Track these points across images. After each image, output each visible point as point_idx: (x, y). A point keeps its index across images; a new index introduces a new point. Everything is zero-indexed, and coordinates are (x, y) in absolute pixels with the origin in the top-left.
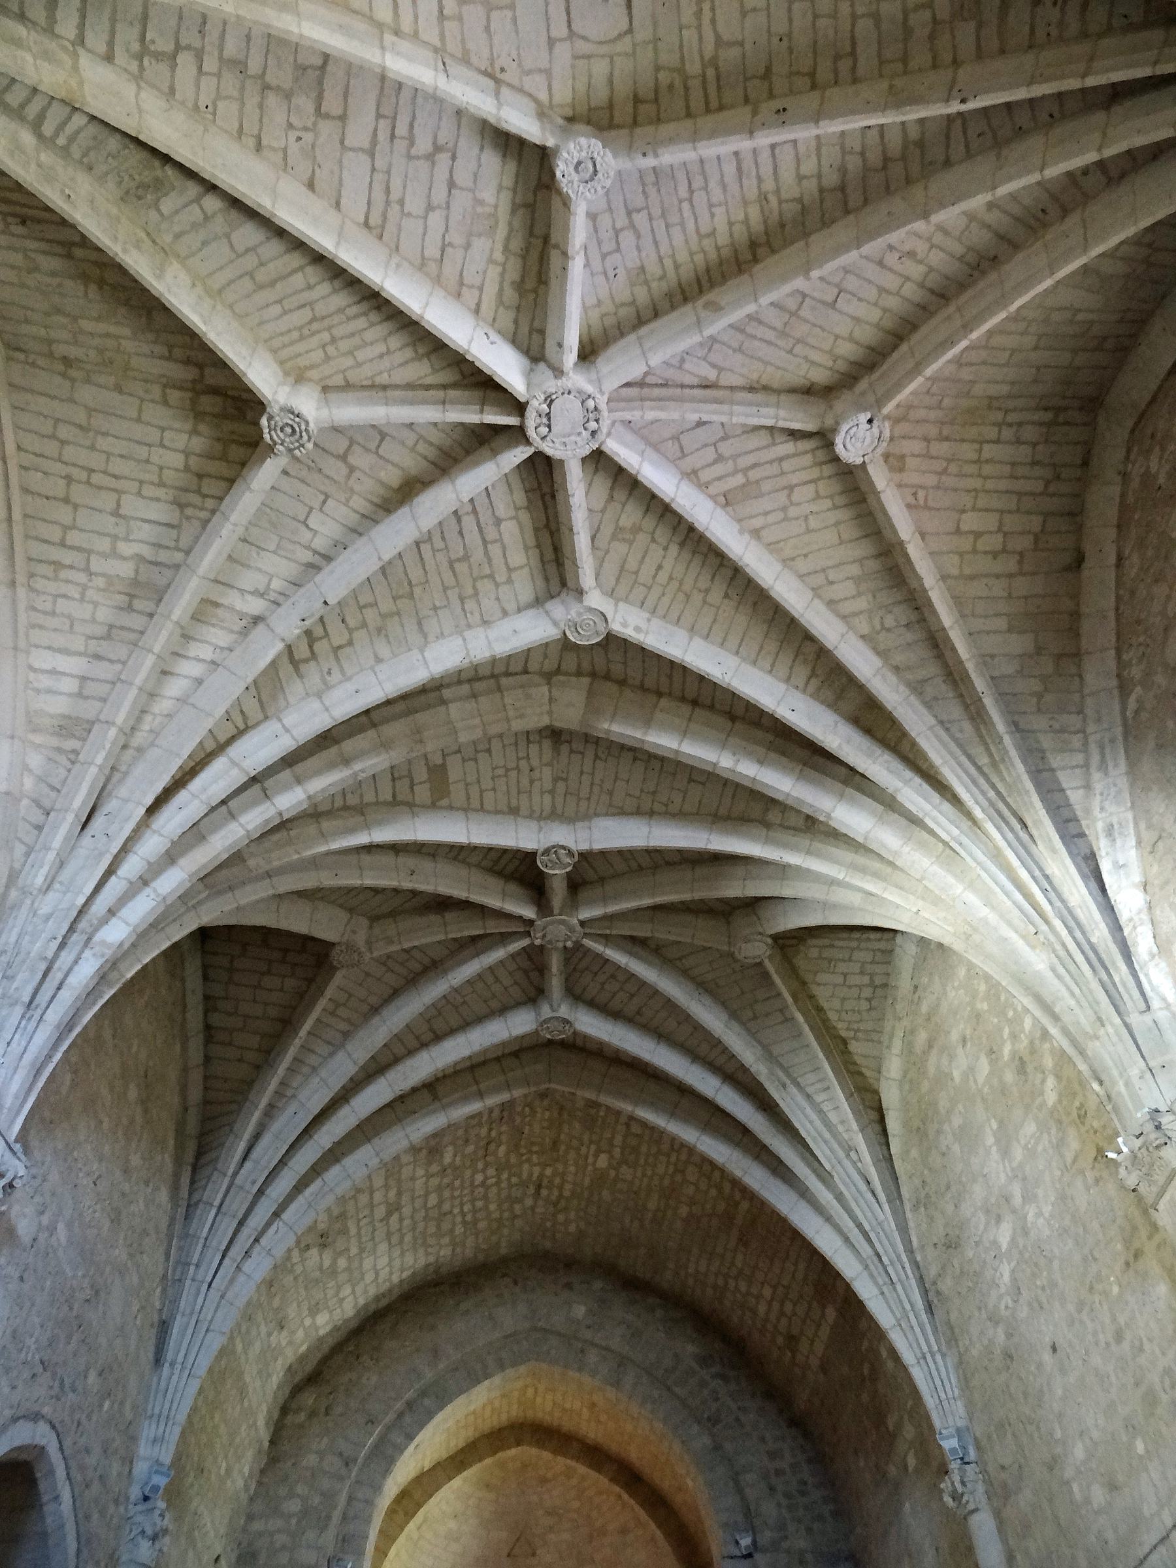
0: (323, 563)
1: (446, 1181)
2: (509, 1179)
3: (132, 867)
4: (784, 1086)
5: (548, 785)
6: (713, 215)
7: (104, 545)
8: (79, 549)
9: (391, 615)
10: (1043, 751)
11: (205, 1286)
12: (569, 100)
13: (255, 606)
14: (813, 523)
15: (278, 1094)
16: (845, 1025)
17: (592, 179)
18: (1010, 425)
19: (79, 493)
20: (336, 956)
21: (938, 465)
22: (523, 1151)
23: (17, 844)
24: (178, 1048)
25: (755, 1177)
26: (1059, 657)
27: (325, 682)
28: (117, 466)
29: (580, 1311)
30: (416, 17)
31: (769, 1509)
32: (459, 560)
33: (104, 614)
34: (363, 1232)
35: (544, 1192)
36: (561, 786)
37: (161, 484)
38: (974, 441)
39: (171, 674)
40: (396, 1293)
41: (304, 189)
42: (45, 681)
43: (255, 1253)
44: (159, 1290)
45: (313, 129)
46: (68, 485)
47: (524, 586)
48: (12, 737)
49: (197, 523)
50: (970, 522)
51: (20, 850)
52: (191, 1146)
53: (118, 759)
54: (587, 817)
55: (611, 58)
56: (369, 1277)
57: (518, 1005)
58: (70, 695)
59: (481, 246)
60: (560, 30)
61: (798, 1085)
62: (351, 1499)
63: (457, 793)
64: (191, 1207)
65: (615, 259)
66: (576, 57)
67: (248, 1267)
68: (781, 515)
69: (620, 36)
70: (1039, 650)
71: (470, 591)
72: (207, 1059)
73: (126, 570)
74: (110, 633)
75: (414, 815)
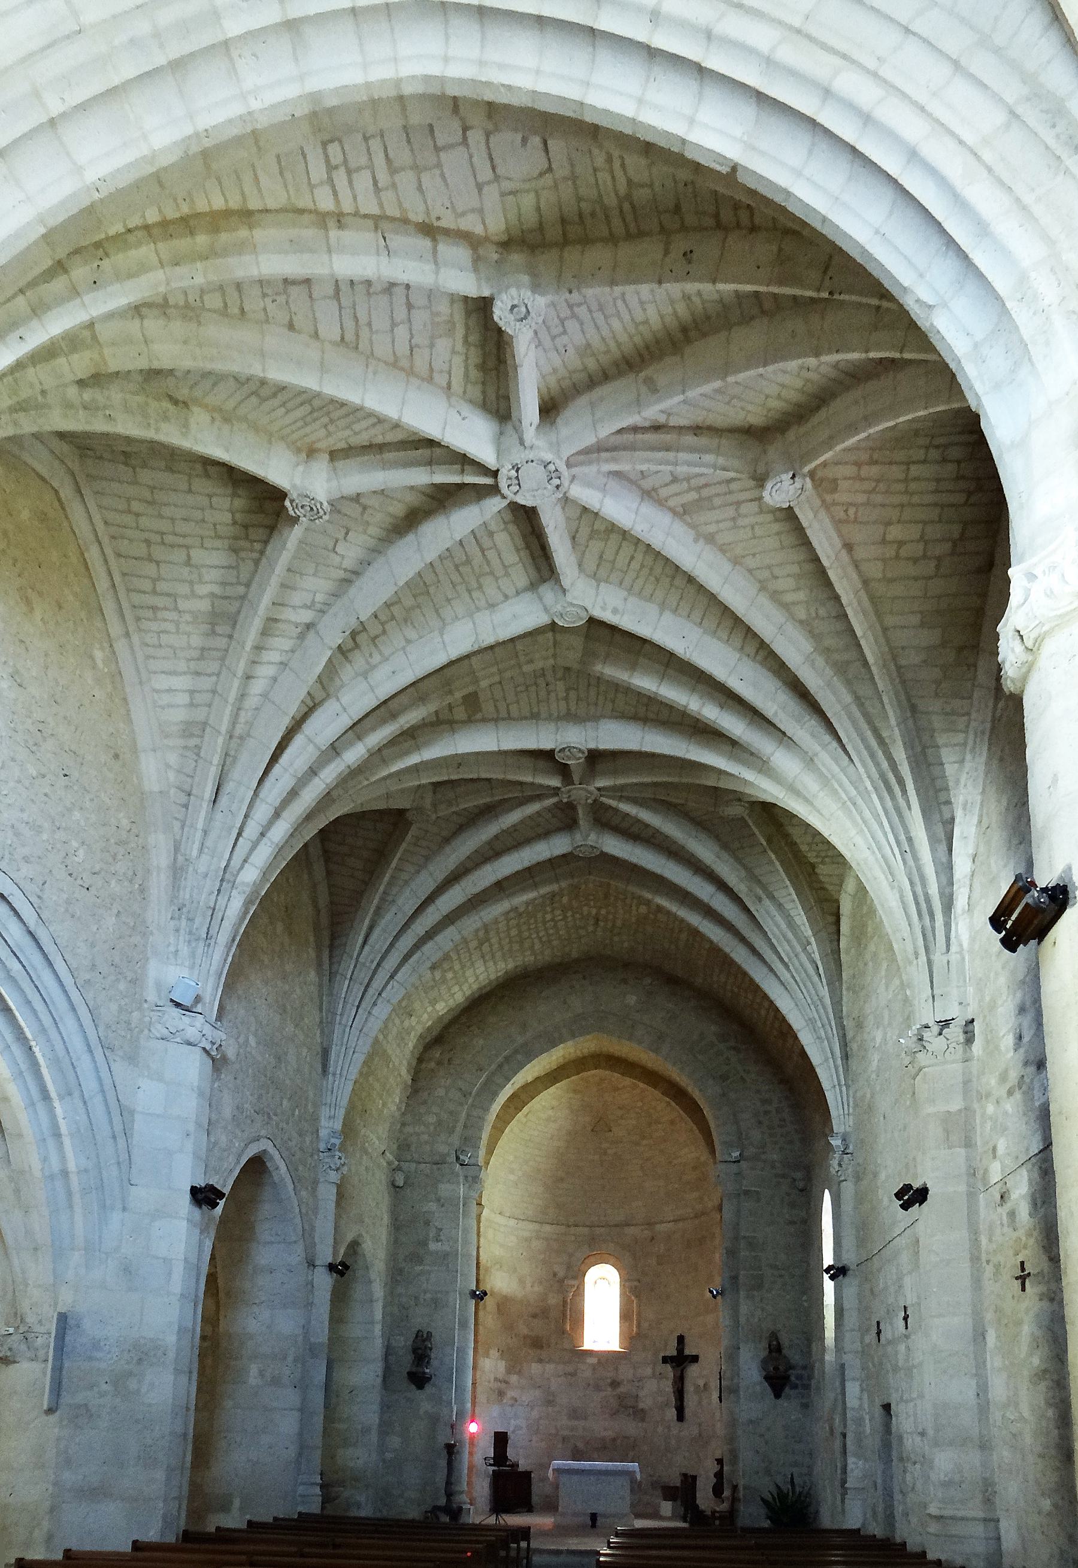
0: (354, 577)
1: (522, 920)
2: (573, 916)
3: (252, 830)
4: (760, 900)
5: (562, 694)
6: (644, 310)
7: (184, 589)
8: (168, 595)
9: (412, 608)
10: (934, 730)
11: (348, 1029)
12: (503, 227)
13: (306, 616)
14: (759, 531)
15: (383, 900)
16: (815, 854)
17: (525, 318)
18: (937, 447)
19: (158, 552)
20: (409, 816)
21: (868, 485)
22: (582, 899)
23: (175, 822)
24: (306, 877)
25: (739, 955)
26: (961, 649)
27: (368, 663)
28: (182, 527)
29: (632, 1000)
30: (355, 198)
31: (756, 1135)
32: (463, 564)
33: (196, 641)
34: (462, 956)
35: (602, 924)
36: (573, 695)
37: (218, 537)
38: (902, 463)
39: (253, 677)
40: (495, 984)
41: (286, 331)
42: (166, 699)
43: (379, 1002)
44: (318, 1032)
45: (285, 292)
46: (149, 546)
47: (520, 577)
48: (154, 750)
49: (251, 563)
50: (895, 532)
51: (177, 825)
52: (326, 934)
53: (228, 748)
54: (596, 718)
55: (537, 192)
56: (471, 980)
57: (559, 830)
58: (185, 706)
59: (443, 345)
60: (486, 174)
61: (772, 897)
62: (468, 1115)
63: (488, 708)
64: (332, 975)
65: (565, 339)
66: (503, 194)
67: (375, 1011)
68: (730, 524)
69: (541, 175)
70: (944, 644)
71: (475, 585)
72: (329, 873)
73: (204, 605)
74: (203, 652)
75: (453, 731)
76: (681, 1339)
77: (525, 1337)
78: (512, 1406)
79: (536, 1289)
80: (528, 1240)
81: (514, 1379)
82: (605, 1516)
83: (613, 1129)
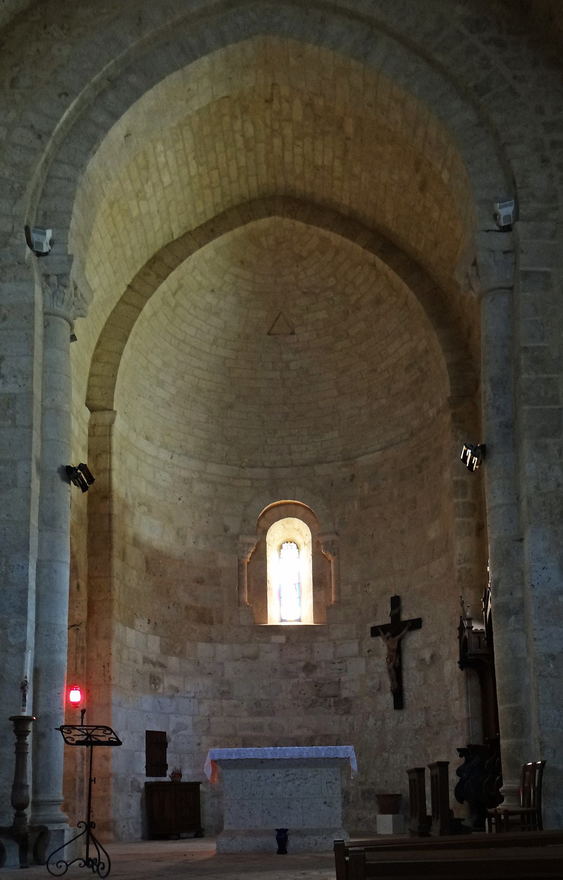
76: (396, 602)
77: (187, 608)
78: (172, 697)
79: (201, 546)
80: (187, 481)
81: (173, 662)
82: (300, 833)
83: (297, 331)
